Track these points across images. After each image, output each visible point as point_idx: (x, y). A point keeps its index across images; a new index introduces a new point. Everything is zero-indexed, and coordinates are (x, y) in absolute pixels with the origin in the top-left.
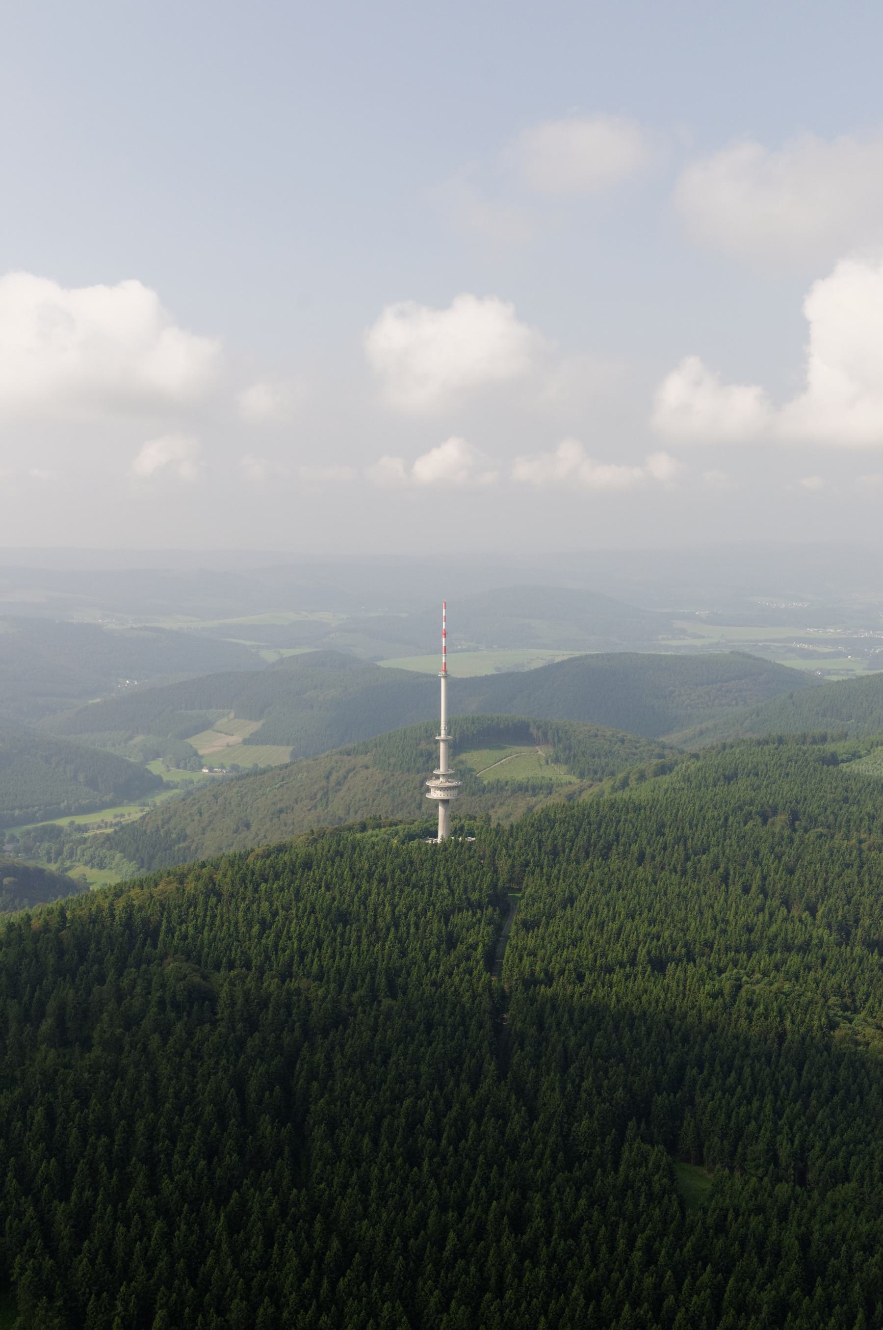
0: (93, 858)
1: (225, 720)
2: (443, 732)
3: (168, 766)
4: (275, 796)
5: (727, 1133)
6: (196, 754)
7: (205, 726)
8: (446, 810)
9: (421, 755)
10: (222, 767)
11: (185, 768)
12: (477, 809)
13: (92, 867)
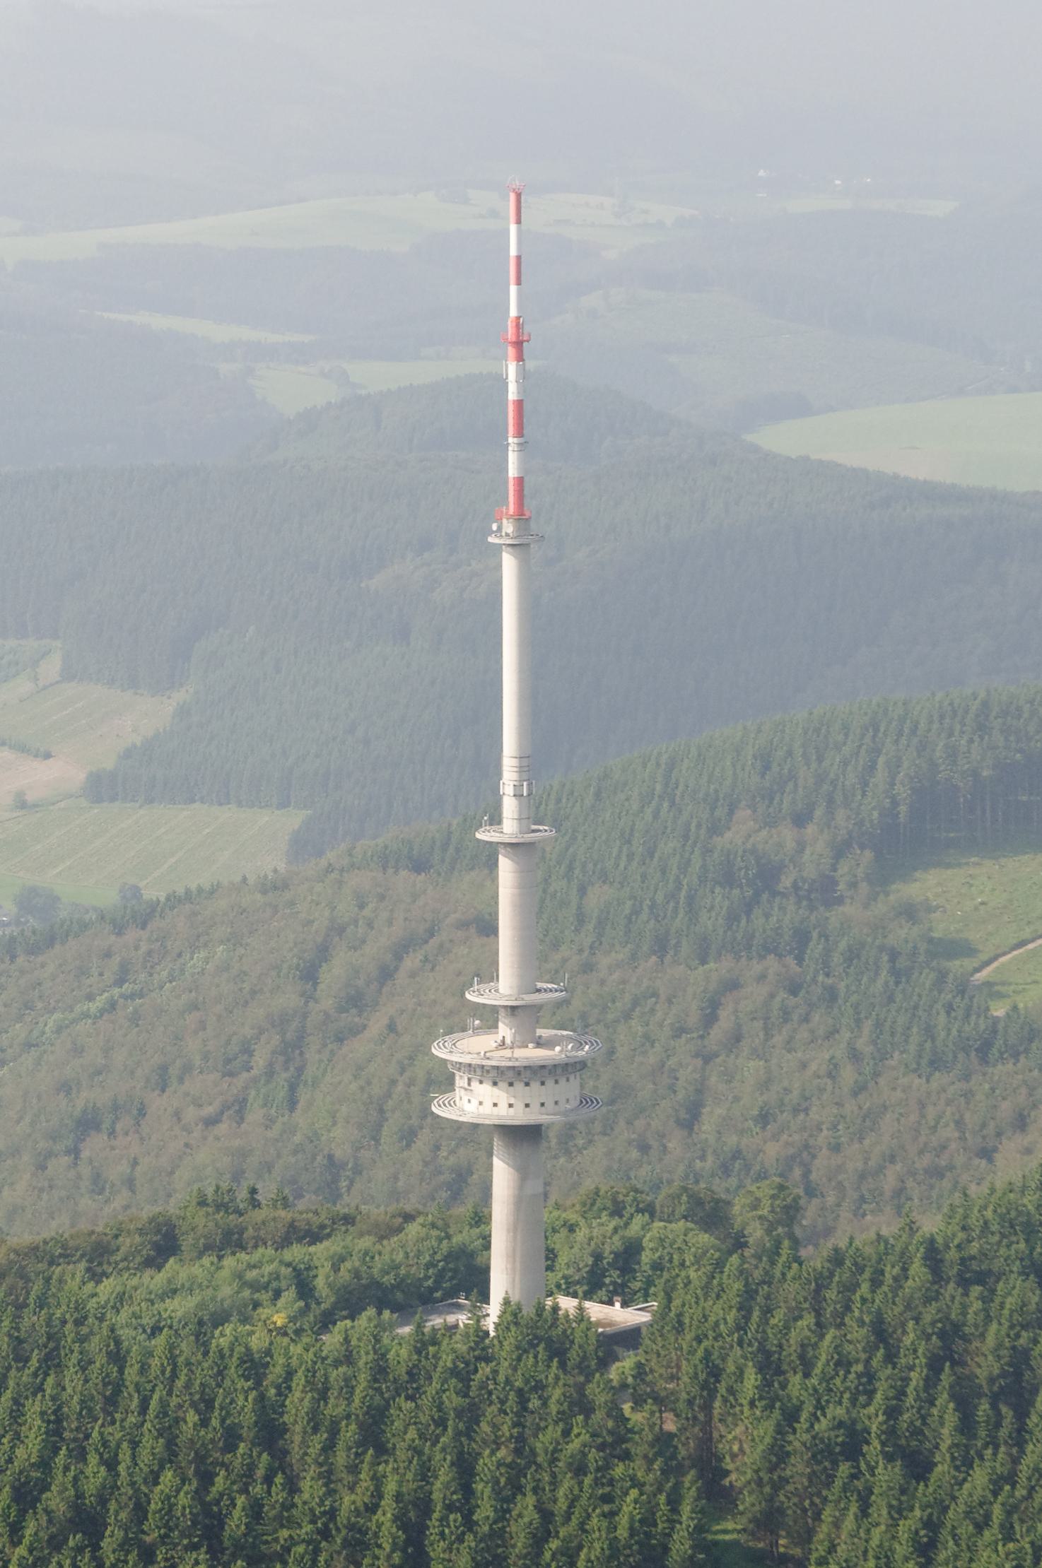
2: (510, 807)
4: (78, 1051)
8: (523, 1173)
9: (729, 879)
12: (949, 1132)
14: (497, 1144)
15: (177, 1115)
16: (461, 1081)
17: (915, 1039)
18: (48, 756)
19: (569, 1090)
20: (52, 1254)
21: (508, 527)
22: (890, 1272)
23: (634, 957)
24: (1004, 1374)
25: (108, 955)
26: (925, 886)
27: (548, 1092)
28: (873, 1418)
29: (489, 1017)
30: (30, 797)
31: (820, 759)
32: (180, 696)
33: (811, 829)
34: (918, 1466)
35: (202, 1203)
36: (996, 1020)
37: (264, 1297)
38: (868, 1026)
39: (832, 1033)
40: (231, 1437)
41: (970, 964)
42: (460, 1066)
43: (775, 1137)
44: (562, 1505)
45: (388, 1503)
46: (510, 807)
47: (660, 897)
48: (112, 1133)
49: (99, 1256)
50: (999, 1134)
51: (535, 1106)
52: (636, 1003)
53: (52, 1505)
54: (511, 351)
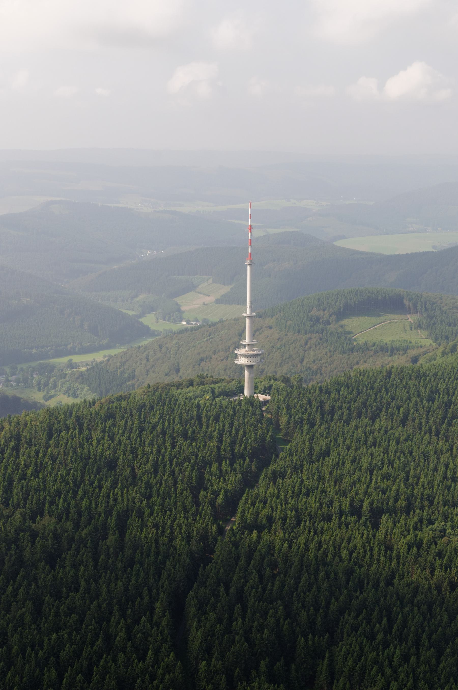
0: (69, 389)
1: (206, 284)
3: (157, 319)
5: (353, 675)
6: (179, 310)
7: (190, 288)
8: (250, 373)
9: (311, 320)
10: (197, 320)
11: (169, 320)
12: (345, 364)
13: (69, 396)
14: (246, 368)
15: (217, 359)
16: (239, 357)
17: (340, 348)
18: (209, 296)
19: (258, 359)
20: (171, 385)
21: (248, 261)
22: (312, 391)
23: (294, 333)
24: (330, 409)
25: (208, 331)
26: (345, 322)
27: (254, 359)
28: (306, 417)
29: (245, 346)
30: (206, 303)
31: (328, 300)
32: (232, 286)
33: (326, 312)
34: (312, 425)
35: (198, 376)
36: (354, 346)
37: (206, 393)
38: (333, 346)
39: (326, 347)
40: (192, 418)
41: (352, 335)
42: (239, 354)
43: (316, 365)
44: (248, 431)
45: (217, 431)
46: (248, 310)
47: (299, 323)
48: (206, 362)
49: (179, 386)
50: (354, 365)
51: (252, 362)
52: (294, 341)
53: (158, 430)
54: (249, 231)
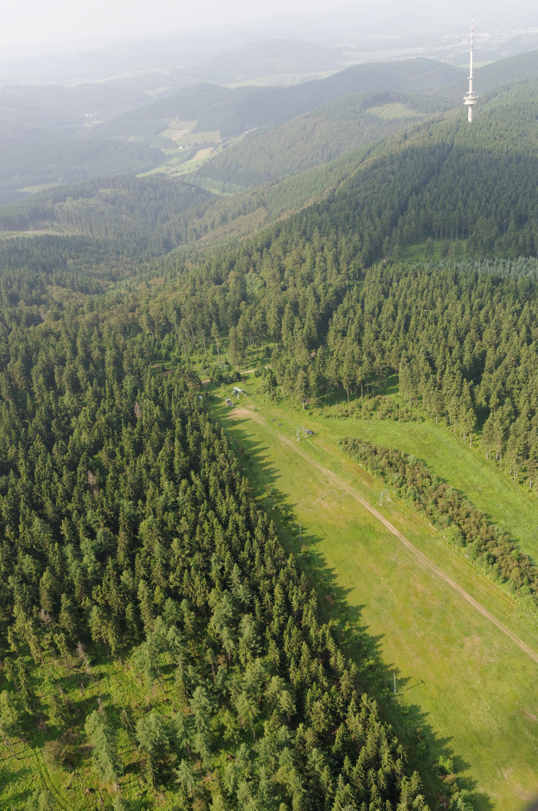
2: (471, 75)
7: (165, 128)
10: (189, 145)
11: (170, 148)
